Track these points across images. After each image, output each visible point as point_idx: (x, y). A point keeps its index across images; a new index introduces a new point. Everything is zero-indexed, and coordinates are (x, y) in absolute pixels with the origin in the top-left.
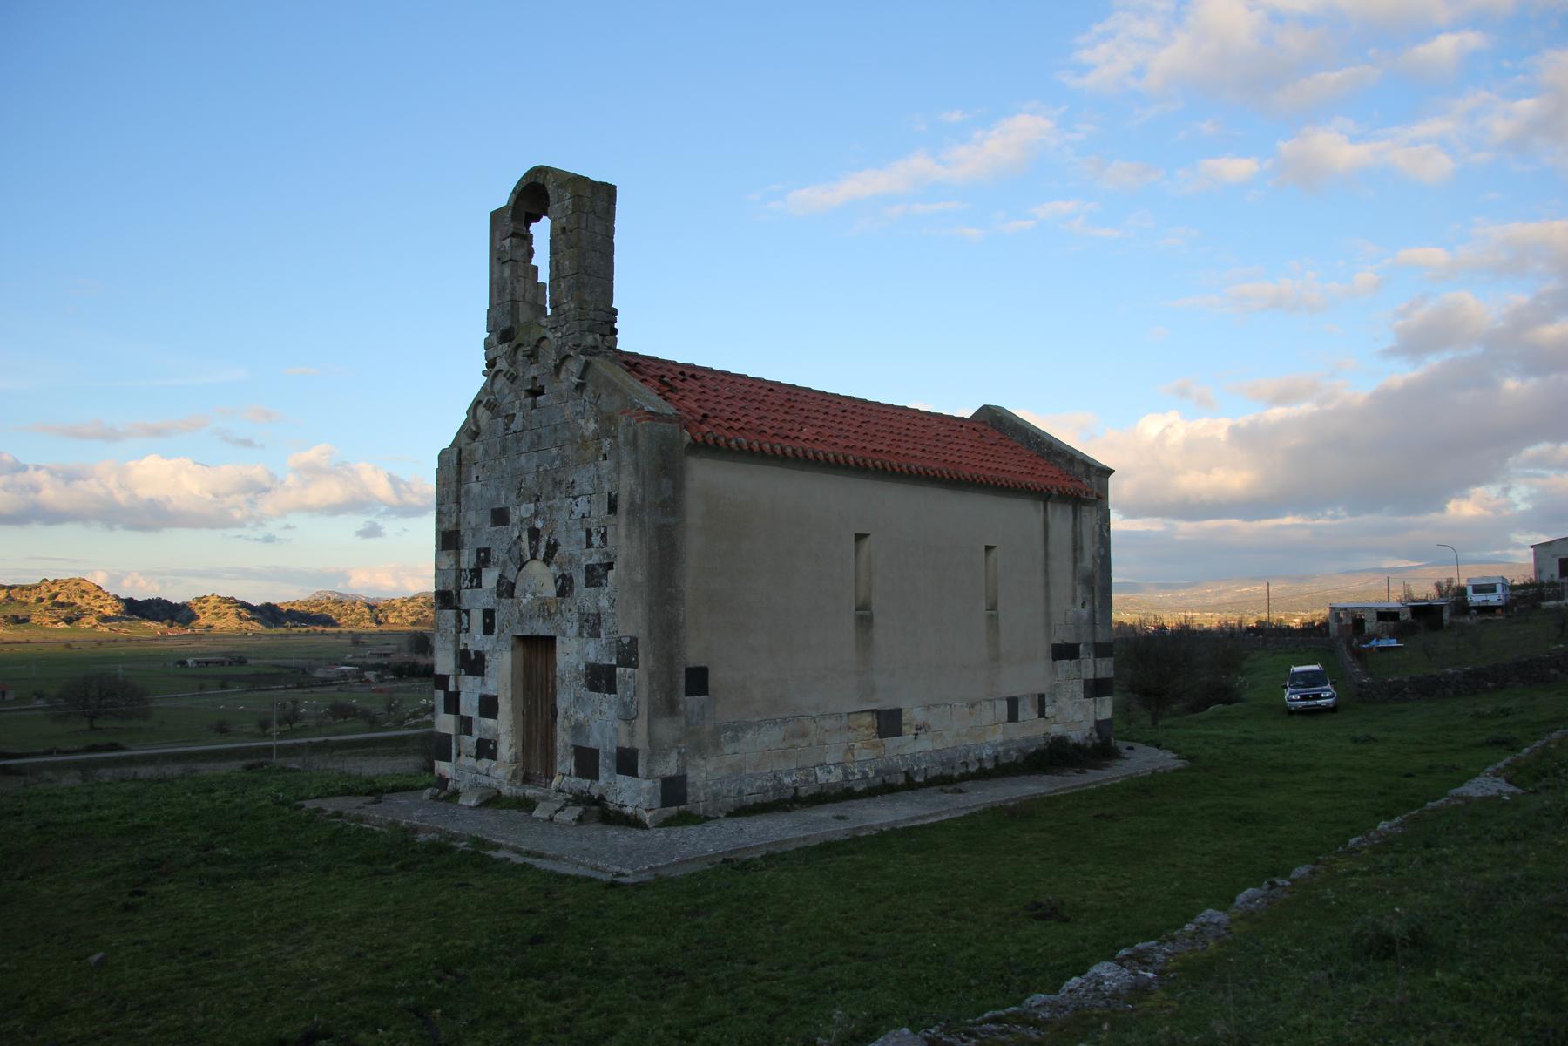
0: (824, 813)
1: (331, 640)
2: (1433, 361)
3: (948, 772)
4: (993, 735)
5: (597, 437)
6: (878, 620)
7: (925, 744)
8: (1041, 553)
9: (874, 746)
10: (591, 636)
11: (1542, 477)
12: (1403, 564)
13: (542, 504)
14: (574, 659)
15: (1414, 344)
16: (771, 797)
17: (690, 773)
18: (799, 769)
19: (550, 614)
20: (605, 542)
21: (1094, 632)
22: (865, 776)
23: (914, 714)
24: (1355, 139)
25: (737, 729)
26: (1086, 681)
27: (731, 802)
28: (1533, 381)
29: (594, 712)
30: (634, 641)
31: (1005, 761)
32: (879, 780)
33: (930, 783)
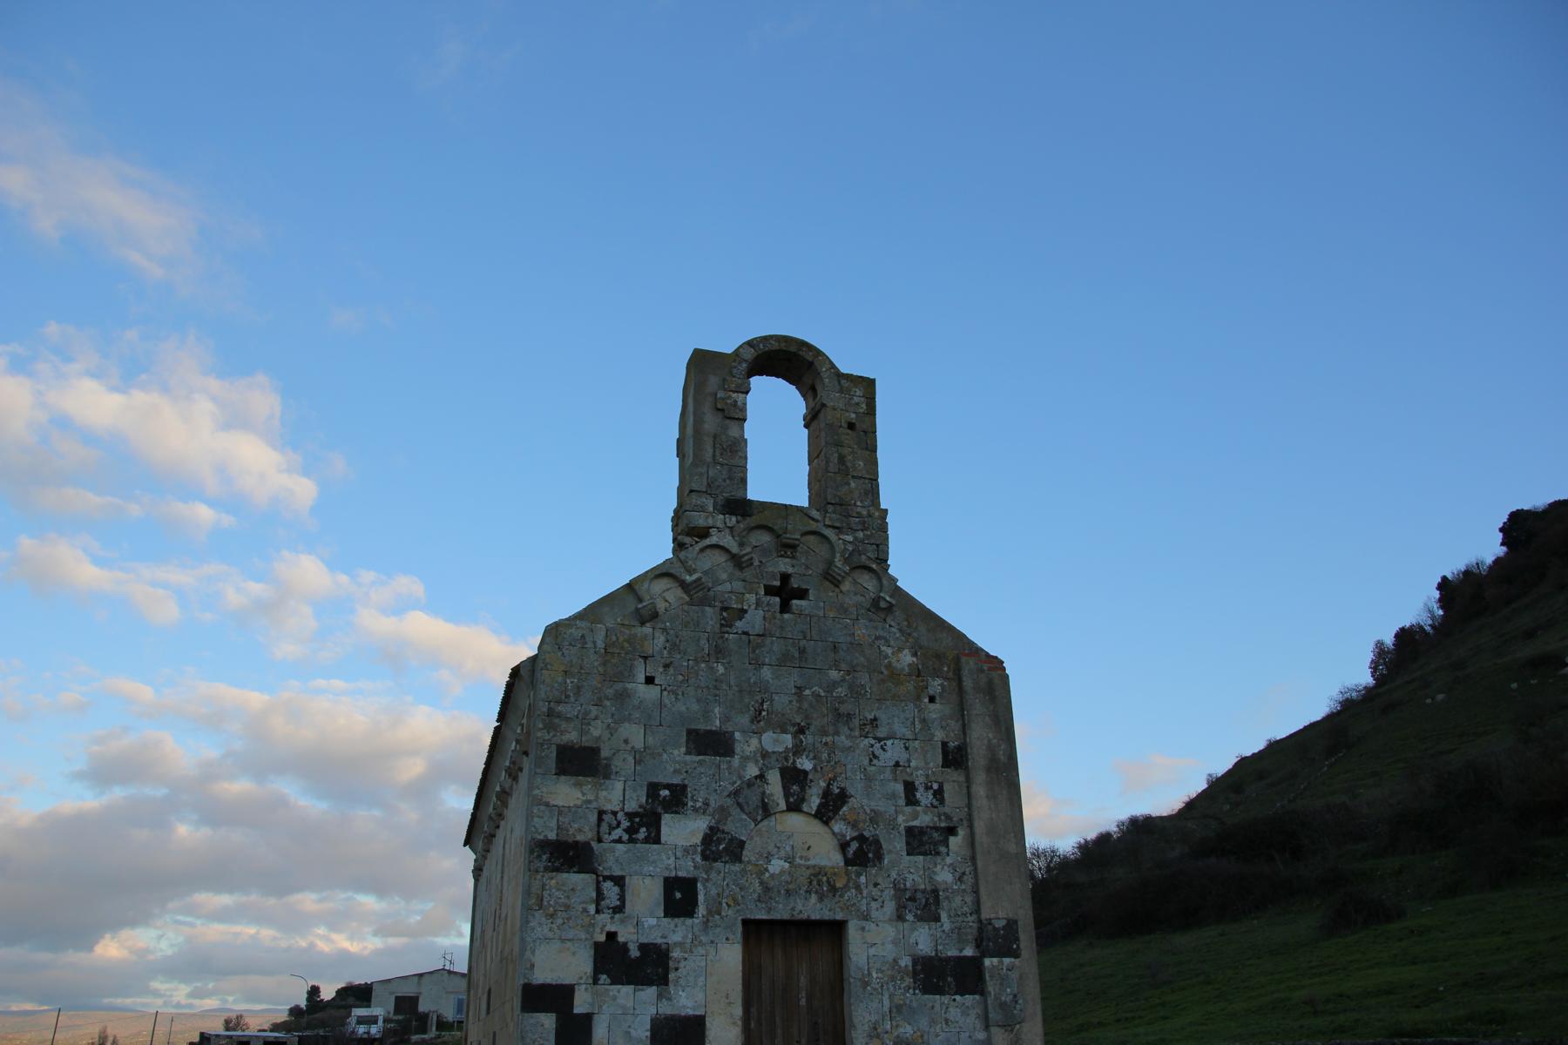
2: (118, 793)
5: (917, 672)
10: (920, 919)
11: (192, 925)
12: (29, 1007)
13: (808, 739)
14: (888, 951)
15: (103, 773)
19: (833, 889)
20: (942, 801)
24: (97, 561)
28: (205, 832)
29: (933, 1022)
30: (1012, 925)
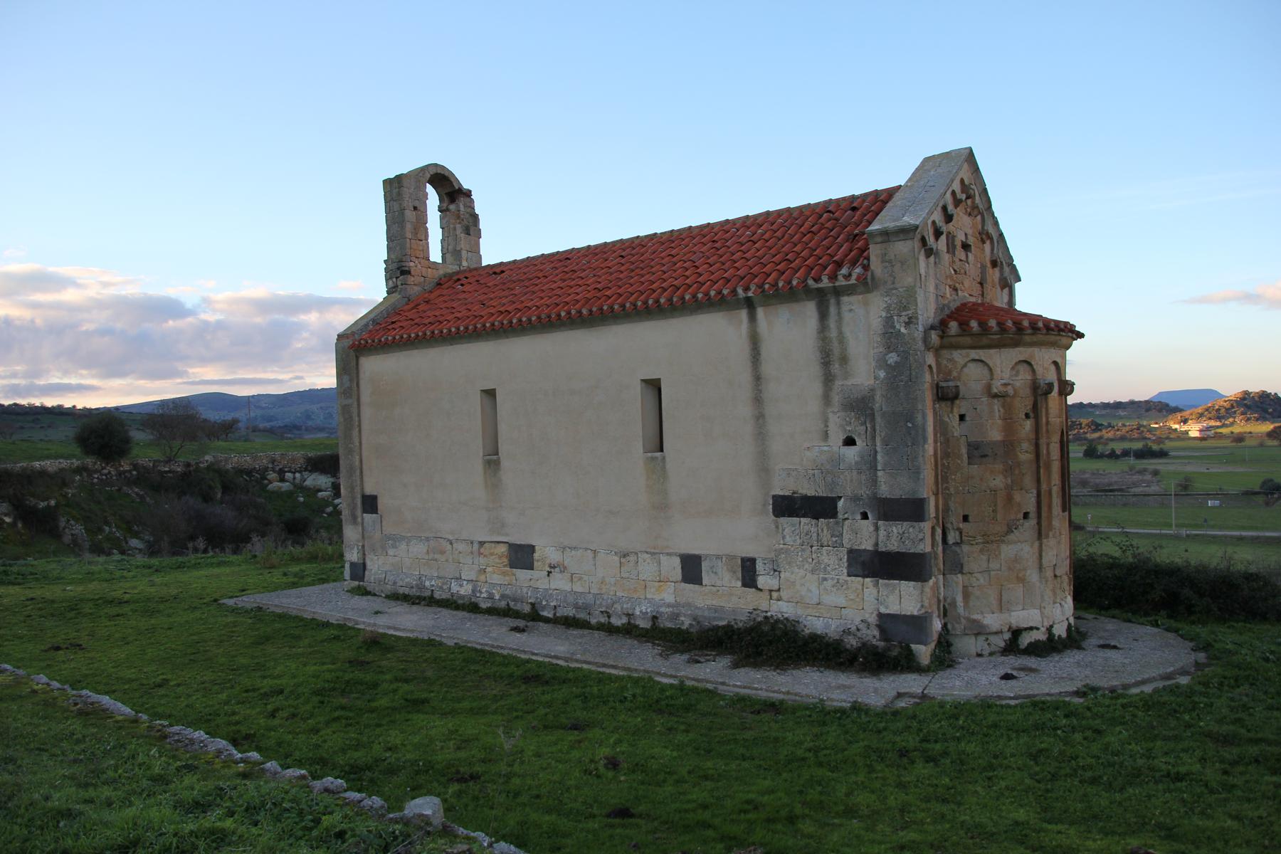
0: (446, 615)
1: (1227, 443)
3: (582, 615)
4: (658, 593)
6: (505, 463)
7: (559, 583)
8: (746, 377)
9: (504, 574)
16: (414, 592)
17: (369, 563)
18: (439, 577)
21: (874, 481)
22: (491, 597)
23: (546, 552)
25: (395, 540)
26: (851, 552)
27: (389, 588)
31: (669, 625)
32: (503, 604)
33: (492, 611)
